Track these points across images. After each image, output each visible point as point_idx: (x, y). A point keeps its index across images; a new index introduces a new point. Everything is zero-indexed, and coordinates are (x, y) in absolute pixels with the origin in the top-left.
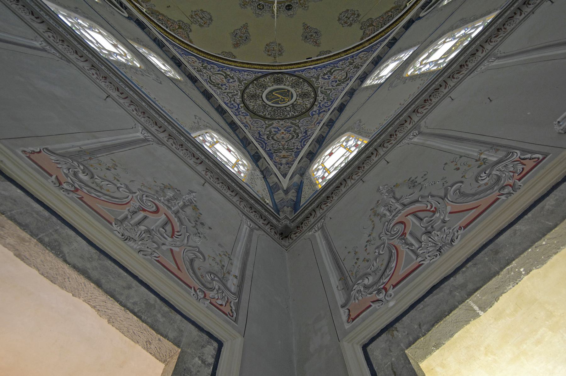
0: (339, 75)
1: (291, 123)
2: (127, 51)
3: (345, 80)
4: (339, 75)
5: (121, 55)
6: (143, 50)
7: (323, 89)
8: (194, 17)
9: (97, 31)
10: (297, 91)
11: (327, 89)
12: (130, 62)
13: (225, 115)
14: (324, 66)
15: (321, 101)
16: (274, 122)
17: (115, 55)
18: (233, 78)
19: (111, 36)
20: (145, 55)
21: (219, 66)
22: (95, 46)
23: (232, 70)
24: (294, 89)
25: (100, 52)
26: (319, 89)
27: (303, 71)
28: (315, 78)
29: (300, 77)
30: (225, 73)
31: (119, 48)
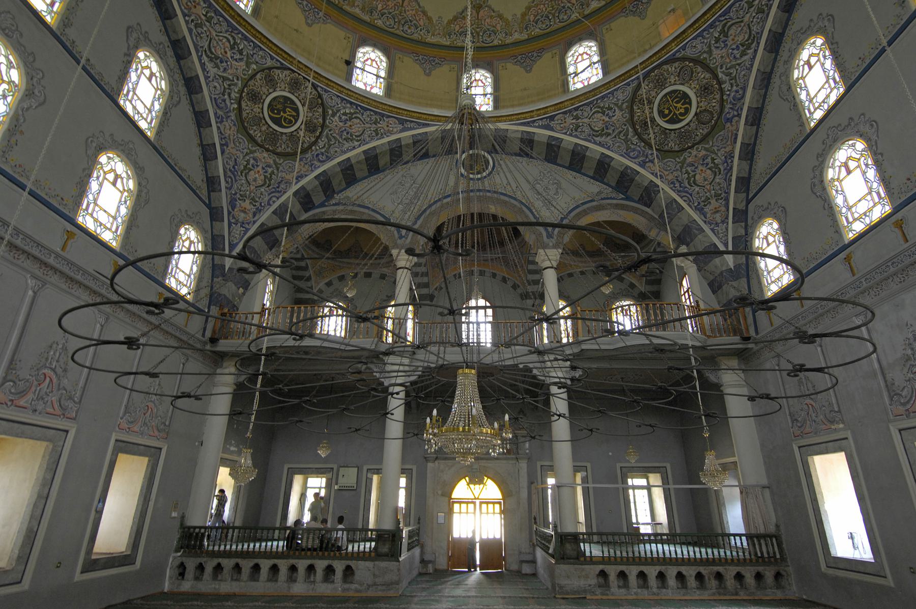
0: (737, 35)
1: (274, 161)
3: (750, 41)
4: (737, 35)
7: (724, 69)
10: (693, 86)
11: (729, 68)
14: (712, 26)
15: (728, 90)
16: (686, 154)
21: (229, 24)
23: (246, 38)
24: (686, 84)
26: (719, 70)
27: (684, 48)
28: (705, 52)
29: (684, 59)
30: (234, 39)
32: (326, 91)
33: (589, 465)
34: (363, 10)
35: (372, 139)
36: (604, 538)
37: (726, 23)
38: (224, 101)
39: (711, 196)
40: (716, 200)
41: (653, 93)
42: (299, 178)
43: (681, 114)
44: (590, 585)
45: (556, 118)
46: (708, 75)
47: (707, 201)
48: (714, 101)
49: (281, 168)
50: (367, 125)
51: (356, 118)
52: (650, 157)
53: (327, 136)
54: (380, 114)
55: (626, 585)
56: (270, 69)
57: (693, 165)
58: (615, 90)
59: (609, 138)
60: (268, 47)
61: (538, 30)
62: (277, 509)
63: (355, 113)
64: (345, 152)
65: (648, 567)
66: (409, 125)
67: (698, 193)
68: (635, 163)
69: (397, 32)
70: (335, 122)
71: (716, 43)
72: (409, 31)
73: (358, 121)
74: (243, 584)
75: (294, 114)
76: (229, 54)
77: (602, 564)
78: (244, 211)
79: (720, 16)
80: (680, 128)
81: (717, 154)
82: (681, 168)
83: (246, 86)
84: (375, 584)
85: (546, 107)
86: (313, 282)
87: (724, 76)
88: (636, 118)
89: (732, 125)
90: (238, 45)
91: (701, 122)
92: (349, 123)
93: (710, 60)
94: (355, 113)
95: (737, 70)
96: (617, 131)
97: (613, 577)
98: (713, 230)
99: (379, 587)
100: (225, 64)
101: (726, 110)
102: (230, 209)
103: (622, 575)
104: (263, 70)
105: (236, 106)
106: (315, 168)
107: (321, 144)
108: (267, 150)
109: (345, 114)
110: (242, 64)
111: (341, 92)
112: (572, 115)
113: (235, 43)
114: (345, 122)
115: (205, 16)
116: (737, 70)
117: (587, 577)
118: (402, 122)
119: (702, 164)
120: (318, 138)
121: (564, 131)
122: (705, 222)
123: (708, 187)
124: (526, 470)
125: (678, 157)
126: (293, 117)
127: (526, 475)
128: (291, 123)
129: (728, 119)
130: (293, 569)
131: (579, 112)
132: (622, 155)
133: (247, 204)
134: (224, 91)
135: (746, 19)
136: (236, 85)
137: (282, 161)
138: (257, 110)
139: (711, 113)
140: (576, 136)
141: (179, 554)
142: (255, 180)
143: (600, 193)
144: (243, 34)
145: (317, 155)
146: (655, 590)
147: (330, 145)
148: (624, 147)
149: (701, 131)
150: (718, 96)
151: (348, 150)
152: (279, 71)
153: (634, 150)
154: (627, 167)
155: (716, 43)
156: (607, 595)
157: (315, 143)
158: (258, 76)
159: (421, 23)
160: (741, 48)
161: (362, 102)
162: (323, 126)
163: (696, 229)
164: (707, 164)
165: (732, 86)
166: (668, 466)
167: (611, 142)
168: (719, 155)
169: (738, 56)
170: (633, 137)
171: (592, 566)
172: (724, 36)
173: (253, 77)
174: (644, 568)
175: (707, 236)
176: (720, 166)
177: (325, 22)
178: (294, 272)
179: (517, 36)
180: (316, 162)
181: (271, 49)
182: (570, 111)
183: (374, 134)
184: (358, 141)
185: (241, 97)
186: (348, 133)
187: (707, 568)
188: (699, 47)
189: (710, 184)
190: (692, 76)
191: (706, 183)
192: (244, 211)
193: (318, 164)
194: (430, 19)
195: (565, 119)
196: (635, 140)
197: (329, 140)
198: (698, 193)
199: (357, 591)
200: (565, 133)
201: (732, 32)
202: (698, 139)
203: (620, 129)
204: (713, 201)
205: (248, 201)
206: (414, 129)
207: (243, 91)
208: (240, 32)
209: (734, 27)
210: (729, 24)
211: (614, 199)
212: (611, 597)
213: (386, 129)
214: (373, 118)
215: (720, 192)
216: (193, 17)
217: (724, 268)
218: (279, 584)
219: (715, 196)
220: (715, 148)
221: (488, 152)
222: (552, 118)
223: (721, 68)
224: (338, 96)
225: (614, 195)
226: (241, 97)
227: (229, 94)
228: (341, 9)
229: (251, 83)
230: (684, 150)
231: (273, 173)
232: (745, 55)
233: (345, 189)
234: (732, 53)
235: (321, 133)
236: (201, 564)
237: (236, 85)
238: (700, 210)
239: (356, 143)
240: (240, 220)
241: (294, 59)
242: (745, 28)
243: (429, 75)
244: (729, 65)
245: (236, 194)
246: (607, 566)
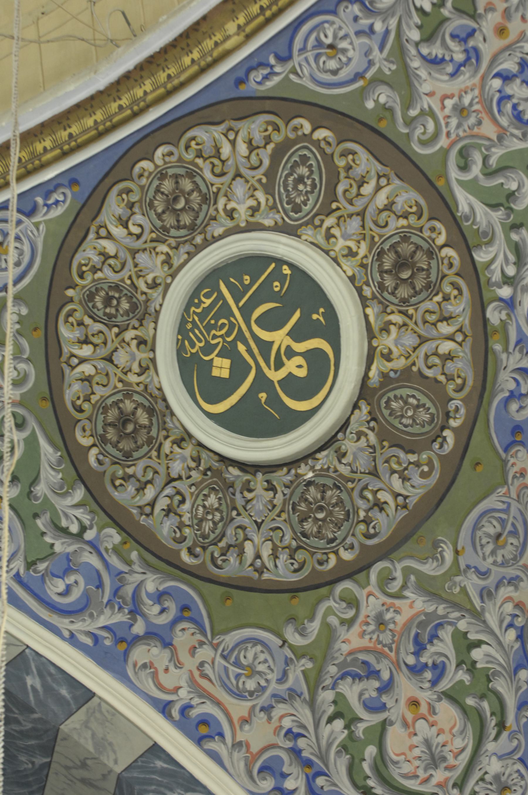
7: (476, 170)
10: (340, 244)
15: (507, 280)
24: (308, 233)
26: (454, 174)
48: (445, 329)
87: (480, 209)
93: (410, 122)
125: (292, 619)
149: (396, 483)
223: (464, 168)
234: (504, 98)
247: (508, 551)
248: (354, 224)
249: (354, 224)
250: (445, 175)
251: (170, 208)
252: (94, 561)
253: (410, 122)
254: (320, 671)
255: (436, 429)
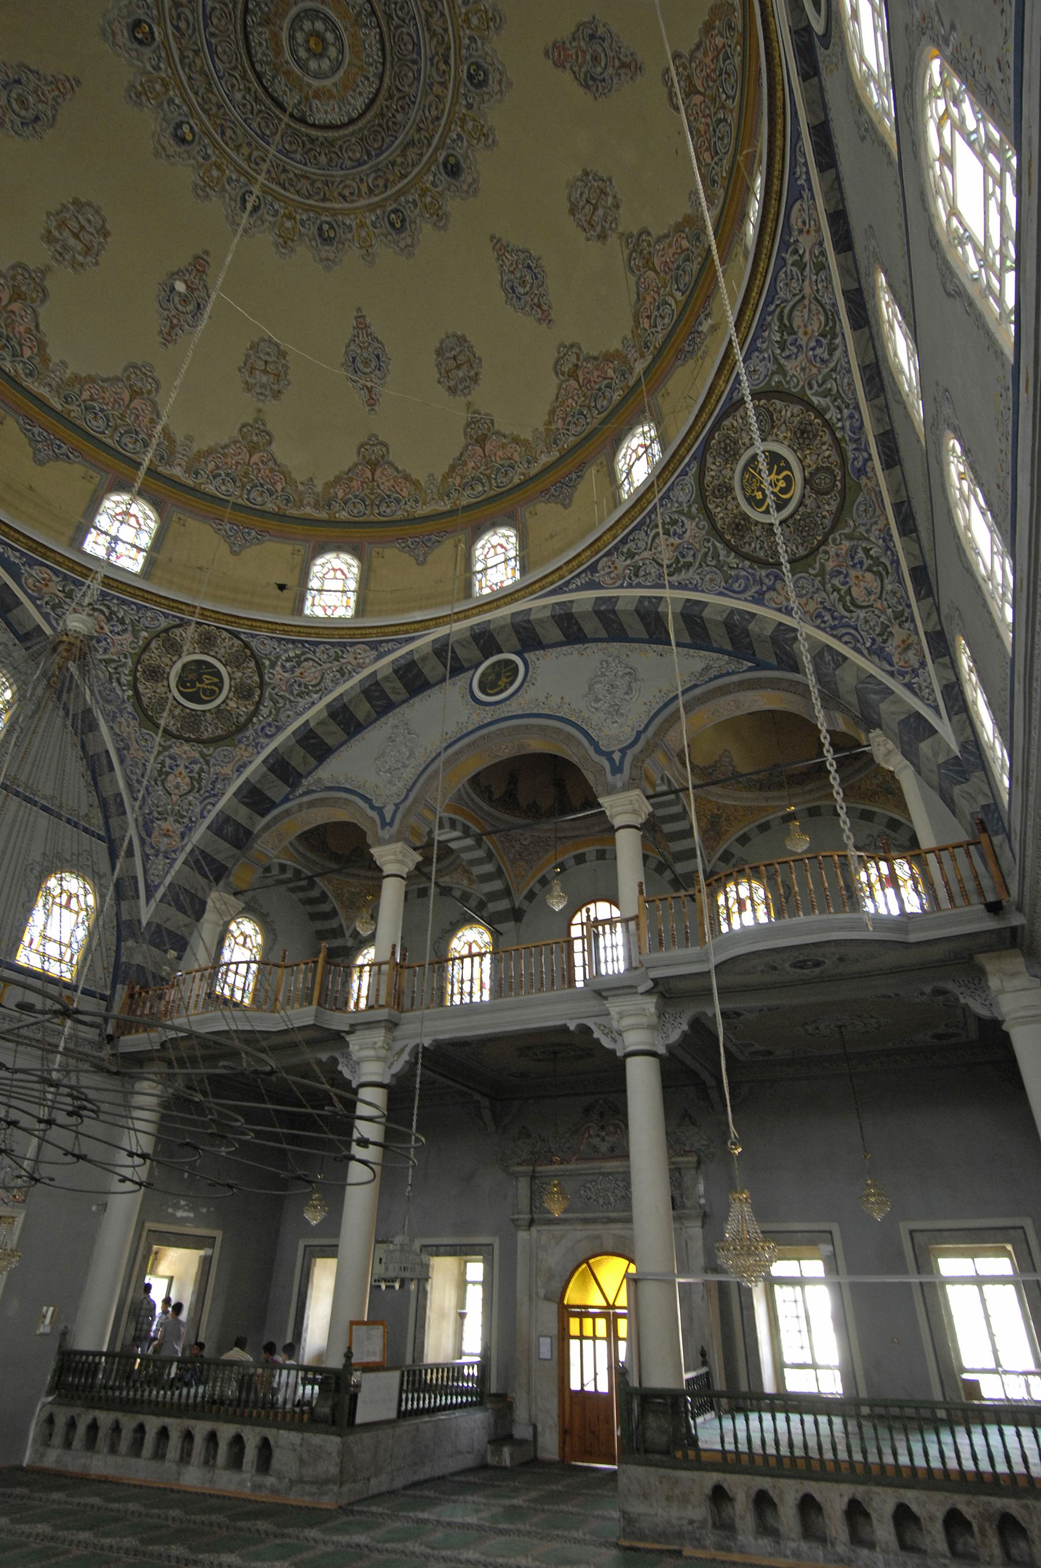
2: (925, 132)
5: (959, 126)
6: (876, 99)
7: (815, 387)
8: (599, 229)
9: (955, 223)
10: (781, 436)
11: (824, 382)
12: (952, 89)
13: (918, 564)
15: (839, 420)
16: (820, 557)
17: (973, 137)
18: (122, 621)
19: (931, 189)
20: (886, 83)
22: (1003, 195)
23: (124, 602)
24: (770, 438)
25: (1009, 169)
26: (809, 392)
28: (773, 373)
30: (108, 607)
31: (942, 149)
32: (253, 636)
33: (835, 1228)
34: (316, 506)
35: (336, 683)
36: (881, 1411)
37: (782, 311)
38: (113, 690)
39: (890, 621)
40: (900, 626)
41: (727, 473)
42: (240, 769)
43: (784, 491)
44: (691, 1522)
45: (600, 567)
46: (797, 409)
47: (885, 632)
48: (824, 447)
49: (212, 761)
50: (325, 666)
51: (306, 660)
52: (766, 581)
53: (272, 699)
54: (339, 644)
55: (766, 1529)
56: (166, 631)
57: (840, 573)
58: (669, 490)
59: (691, 570)
60: (156, 603)
61: (572, 438)
62: (286, 1322)
63: (303, 653)
64: (301, 714)
65: (823, 1484)
66: (385, 647)
67: (867, 622)
68: (746, 600)
69: (372, 518)
70: (277, 675)
71: (783, 350)
72: (388, 511)
73: (311, 663)
74: (119, 1460)
75: (216, 680)
76: (107, 630)
77: (718, 1470)
78: (167, 835)
79: (766, 305)
80: (791, 516)
81: (868, 539)
82: (823, 583)
83: (138, 662)
84: (301, 1481)
85: (579, 555)
86: (342, 918)
87: (821, 400)
88: (719, 524)
89: (868, 478)
90: (115, 613)
91: (820, 493)
92: (298, 671)
93: (788, 383)
94: (303, 653)
95: (835, 380)
96: (699, 556)
97: (742, 1507)
98: (909, 686)
99: (308, 1488)
100: (104, 643)
101: (850, 455)
102: (144, 834)
103: (763, 1501)
104: (158, 636)
105: (130, 693)
106: (262, 748)
107: (264, 711)
108: (188, 740)
109: (289, 659)
110: (128, 636)
111: (273, 631)
112: (622, 553)
113: (112, 612)
114: (292, 670)
115: (63, 591)
116: (835, 380)
117: (684, 1500)
118: (373, 646)
119: (854, 566)
120: (258, 704)
121: (619, 583)
122: (891, 674)
123: (878, 605)
124: (700, 1243)
125: (810, 566)
126: (215, 684)
127: (701, 1253)
128: (213, 694)
129: (859, 470)
130: (188, 1436)
131: (631, 545)
132: (720, 594)
133: (169, 825)
134: (111, 678)
135: (807, 291)
136: (124, 665)
137: (212, 749)
138: (161, 690)
139: (829, 470)
140: (639, 586)
141: (50, 1399)
142: (177, 786)
143: (707, 668)
144: (118, 598)
145: (263, 729)
146: (840, 1549)
147: (278, 710)
148: (719, 578)
149: (827, 507)
150: (827, 438)
151: (306, 709)
152: (180, 630)
153: (737, 578)
154: (733, 611)
155: (783, 350)
156: (729, 1550)
157: (256, 712)
158: (154, 645)
159: (405, 493)
160: (824, 341)
161: (308, 635)
162: (262, 685)
163: (875, 692)
164: (861, 563)
165: (841, 412)
166: (1028, 1224)
167: (697, 577)
168: (873, 539)
169: (826, 356)
170: (728, 556)
171: (696, 1475)
172: (789, 334)
173: (146, 647)
174: (814, 1488)
175: (900, 701)
176: (883, 560)
177: (260, 542)
178: (308, 907)
179: (544, 459)
180: (262, 740)
181: (160, 604)
182: (616, 548)
183: (338, 676)
184: (316, 692)
185: (136, 679)
186: (300, 685)
187: (975, 1499)
188: (761, 368)
189: (880, 598)
190: (773, 421)
191: (872, 597)
192: (167, 835)
193: (267, 740)
194: (416, 483)
195: (613, 563)
196: (732, 560)
197: (275, 702)
198: (867, 622)
199: (275, 1491)
200: (621, 586)
201: (797, 322)
202: (828, 522)
203: (704, 550)
204: (895, 629)
205: (171, 819)
206: (393, 651)
207: (136, 670)
208: (114, 597)
209: (796, 313)
210: (786, 311)
211: (733, 673)
212: (736, 1557)
213: (354, 662)
214: (332, 652)
215: (901, 608)
216: (47, 599)
217: (941, 759)
218: (167, 1464)
219: (896, 618)
220: (862, 529)
221: (516, 653)
222: (593, 568)
223: (811, 388)
224: (272, 638)
225: (732, 667)
226: (136, 679)
227: (118, 681)
228: (285, 516)
229: (145, 656)
230: (814, 551)
231: (202, 770)
232: (835, 349)
233: (316, 768)
234: (815, 356)
235: (261, 696)
236: (73, 1417)
237: (124, 665)
238: (878, 653)
239: (315, 696)
240: (163, 849)
241: (195, 607)
242: (813, 307)
243: (421, 563)
244: (820, 378)
245: (150, 813)
246: (728, 1476)
247: (870, 513)
248: (783, 427)
249: (783, 427)
250: (805, 394)
251: (726, 452)
252: (743, 573)
253: (788, 383)
254: (824, 579)
255: (457, 626)
